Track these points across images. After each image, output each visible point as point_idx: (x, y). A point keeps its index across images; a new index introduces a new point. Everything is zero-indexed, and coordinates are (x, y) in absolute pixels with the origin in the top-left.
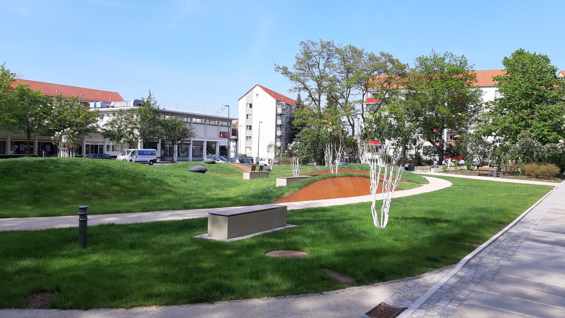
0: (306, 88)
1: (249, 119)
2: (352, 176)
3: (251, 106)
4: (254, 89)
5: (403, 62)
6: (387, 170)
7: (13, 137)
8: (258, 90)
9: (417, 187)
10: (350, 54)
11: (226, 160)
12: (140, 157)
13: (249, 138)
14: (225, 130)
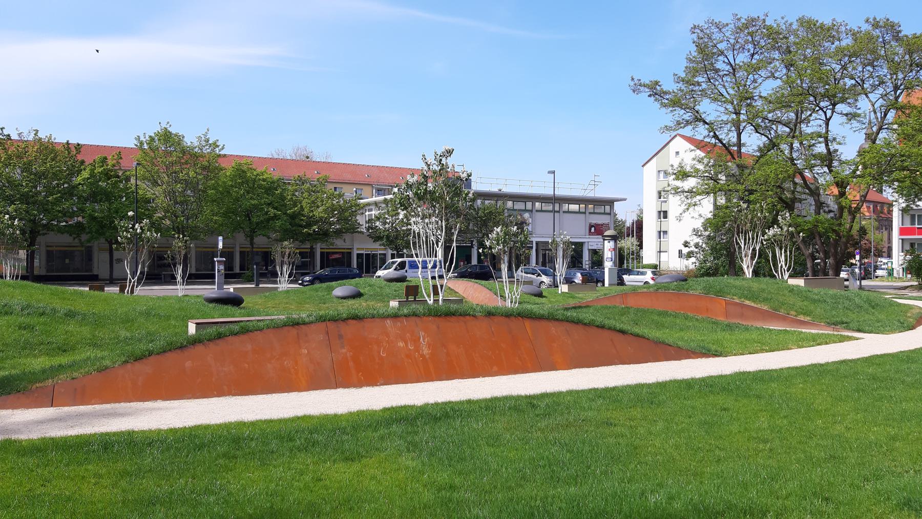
4: (671, 144)
7: (242, 245)
12: (413, 272)
13: (662, 233)
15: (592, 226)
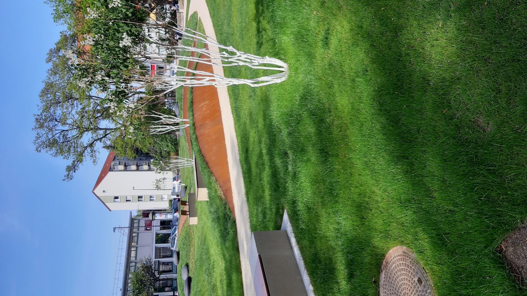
0: (91, 145)
1: (131, 199)
2: (192, 102)
3: (116, 198)
5: (58, 38)
6: (185, 57)
8: (98, 191)
9: (202, 24)
10: (50, 97)
11: (175, 227)
13: (151, 198)
14: (142, 223)
15: (146, 228)
